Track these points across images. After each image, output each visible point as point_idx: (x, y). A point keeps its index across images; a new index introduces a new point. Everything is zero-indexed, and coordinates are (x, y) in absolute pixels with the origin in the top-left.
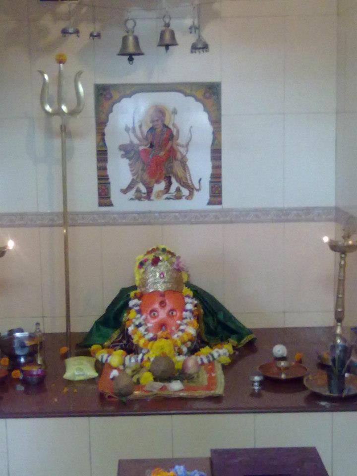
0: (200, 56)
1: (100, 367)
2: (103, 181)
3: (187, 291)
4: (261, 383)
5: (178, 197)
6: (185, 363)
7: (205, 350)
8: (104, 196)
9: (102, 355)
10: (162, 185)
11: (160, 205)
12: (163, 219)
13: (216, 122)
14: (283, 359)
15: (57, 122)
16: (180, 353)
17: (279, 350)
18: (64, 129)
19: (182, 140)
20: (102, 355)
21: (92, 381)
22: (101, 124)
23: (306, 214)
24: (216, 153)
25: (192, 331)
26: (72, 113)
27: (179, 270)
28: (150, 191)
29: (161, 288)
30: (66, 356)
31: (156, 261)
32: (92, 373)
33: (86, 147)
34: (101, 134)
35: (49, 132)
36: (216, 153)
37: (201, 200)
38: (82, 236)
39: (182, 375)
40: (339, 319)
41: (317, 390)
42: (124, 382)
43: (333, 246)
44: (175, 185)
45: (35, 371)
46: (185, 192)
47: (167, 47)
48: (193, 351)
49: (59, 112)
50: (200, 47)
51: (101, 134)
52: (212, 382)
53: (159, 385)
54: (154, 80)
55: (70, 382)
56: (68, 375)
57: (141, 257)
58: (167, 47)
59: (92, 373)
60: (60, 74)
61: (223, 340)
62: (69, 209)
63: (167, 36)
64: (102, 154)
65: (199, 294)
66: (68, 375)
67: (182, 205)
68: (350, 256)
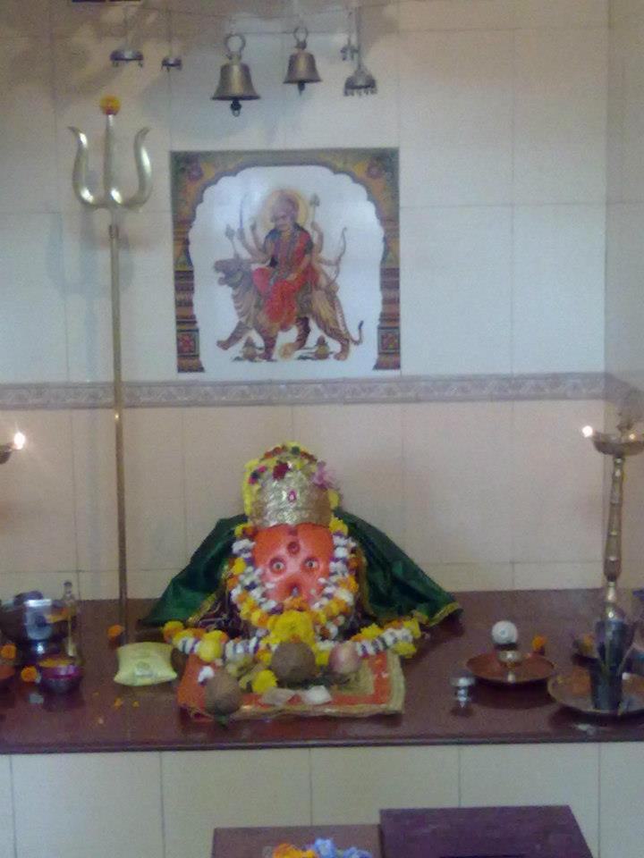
0: (360, 101)
1: (181, 661)
2: (187, 326)
3: (337, 525)
4: (471, 690)
5: (322, 354)
6: (333, 655)
7: (371, 631)
8: (188, 354)
9: (184, 640)
10: (292, 334)
11: (288, 369)
12: (294, 394)
13: (390, 220)
14: (510, 646)
15: (102, 220)
16: (324, 636)
17: (504, 631)
18: (115, 232)
19: (328, 252)
20: (184, 640)
21: (166, 686)
22: (182, 224)
23: (552, 386)
24: (390, 276)
25: (346, 596)
26: (130, 204)
27: (323, 487)
28: (270, 343)
29: (290, 518)
30: (118, 642)
31: (281, 471)
32: (167, 673)
33: (156, 266)
34: (182, 242)
35: (88, 238)
36: (390, 276)
37: (362, 361)
38: (149, 426)
39: (328, 676)
40: (612, 574)
41: (572, 703)
42: (224, 689)
43: (602, 444)
44: (316, 333)
45: (64, 668)
46: (334, 346)
47: (301, 84)
48: (348, 633)
49: (106, 202)
50: (361, 84)
51: (182, 242)
52: (382, 689)
53: (287, 693)
54: (277, 145)
55: (126, 689)
56: (123, 676)
57: (254, 464)
58: (301, 84)
59: (167, 673)
60: (108, 134)
61: (403, 613)
62: (125, 377)
63: (302, 66)
64: (184, 279)
65: (358, 530)
66: (123, 676)
67: (329, 369)
68: (632, 462)
